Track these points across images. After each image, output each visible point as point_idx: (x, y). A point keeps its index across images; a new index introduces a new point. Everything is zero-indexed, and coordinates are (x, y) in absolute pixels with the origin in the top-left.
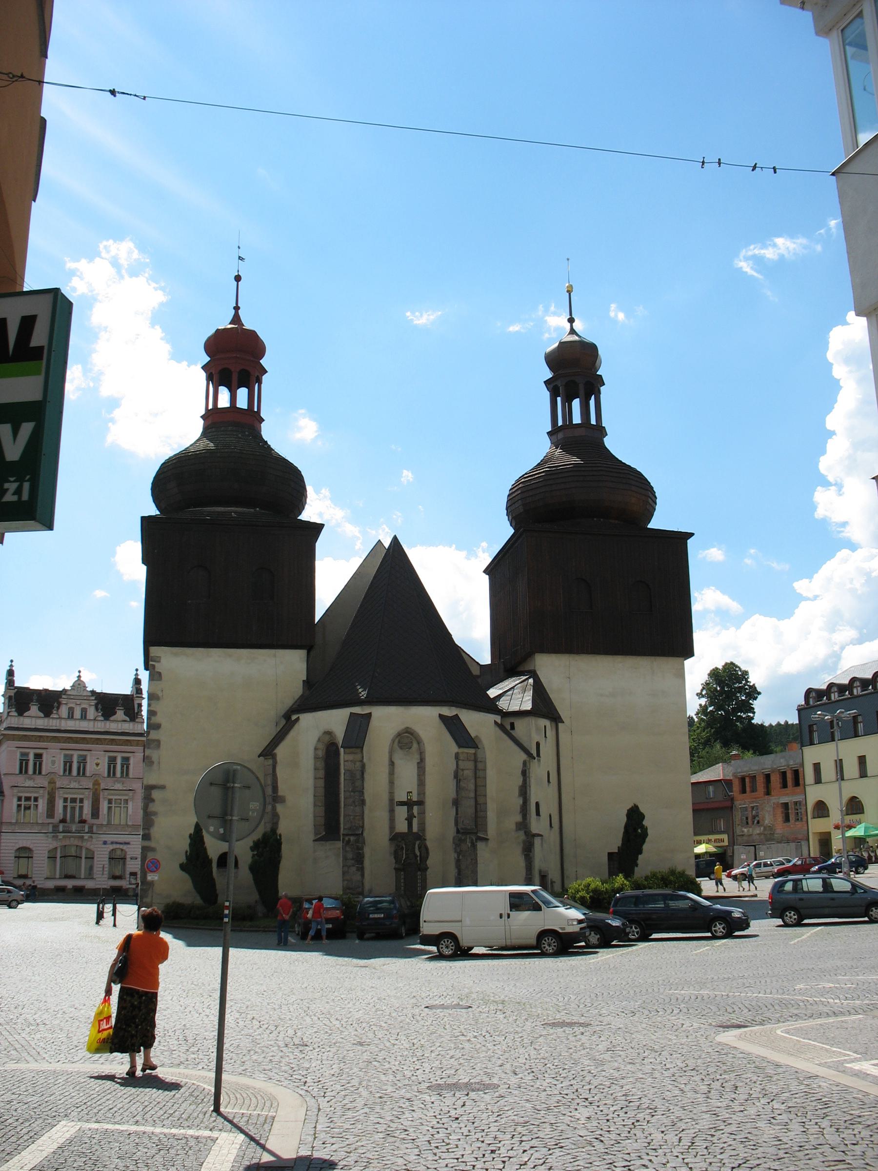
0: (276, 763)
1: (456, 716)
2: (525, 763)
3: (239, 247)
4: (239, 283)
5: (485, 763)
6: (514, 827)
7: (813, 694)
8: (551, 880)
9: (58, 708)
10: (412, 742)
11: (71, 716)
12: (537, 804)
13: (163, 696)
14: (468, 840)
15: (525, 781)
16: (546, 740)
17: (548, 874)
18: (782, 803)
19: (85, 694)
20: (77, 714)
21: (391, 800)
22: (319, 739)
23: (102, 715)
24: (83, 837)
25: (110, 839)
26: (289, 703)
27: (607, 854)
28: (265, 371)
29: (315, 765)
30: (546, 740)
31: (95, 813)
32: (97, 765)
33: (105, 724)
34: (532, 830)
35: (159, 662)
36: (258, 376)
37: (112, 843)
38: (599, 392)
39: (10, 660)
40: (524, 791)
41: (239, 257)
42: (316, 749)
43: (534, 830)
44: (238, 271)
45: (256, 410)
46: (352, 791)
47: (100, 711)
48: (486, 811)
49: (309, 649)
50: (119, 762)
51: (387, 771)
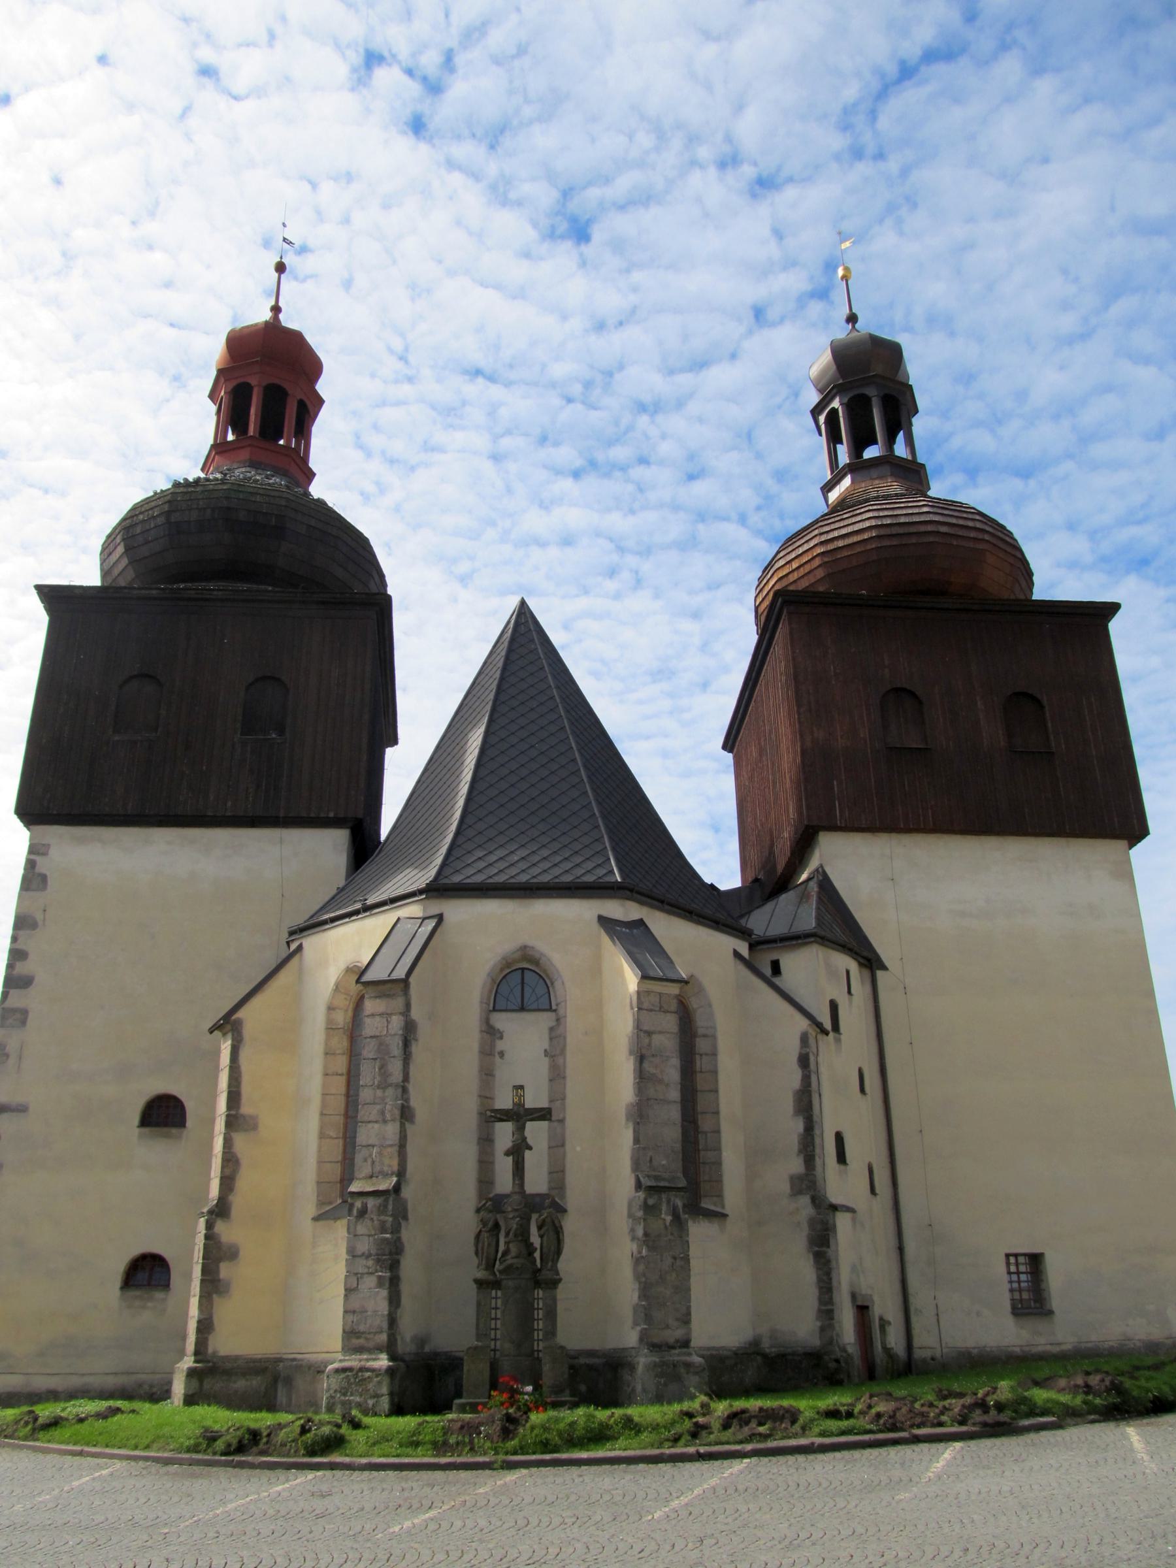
1: (640, 923)
2: (804, 1039)
4: (282, 275)
5: (714, 1037)
6: (786, 1187)
8: (881, 1319)
12: (839, 1138)
13: (44, 920)
14: (664, 1208)
15: (806, 1080)
16: (850, 1002)
17: (873, 1301)
22: (337, 987)
29: (326, 1044)
30: (850, 1002)
34: (828, 1195)
35: (45, 854)
38: (911, 424)
42: (331, 1008)
43: (834, 1197)
46: (378, 1087)
48: (718, 1149)
51: (476, 1046)
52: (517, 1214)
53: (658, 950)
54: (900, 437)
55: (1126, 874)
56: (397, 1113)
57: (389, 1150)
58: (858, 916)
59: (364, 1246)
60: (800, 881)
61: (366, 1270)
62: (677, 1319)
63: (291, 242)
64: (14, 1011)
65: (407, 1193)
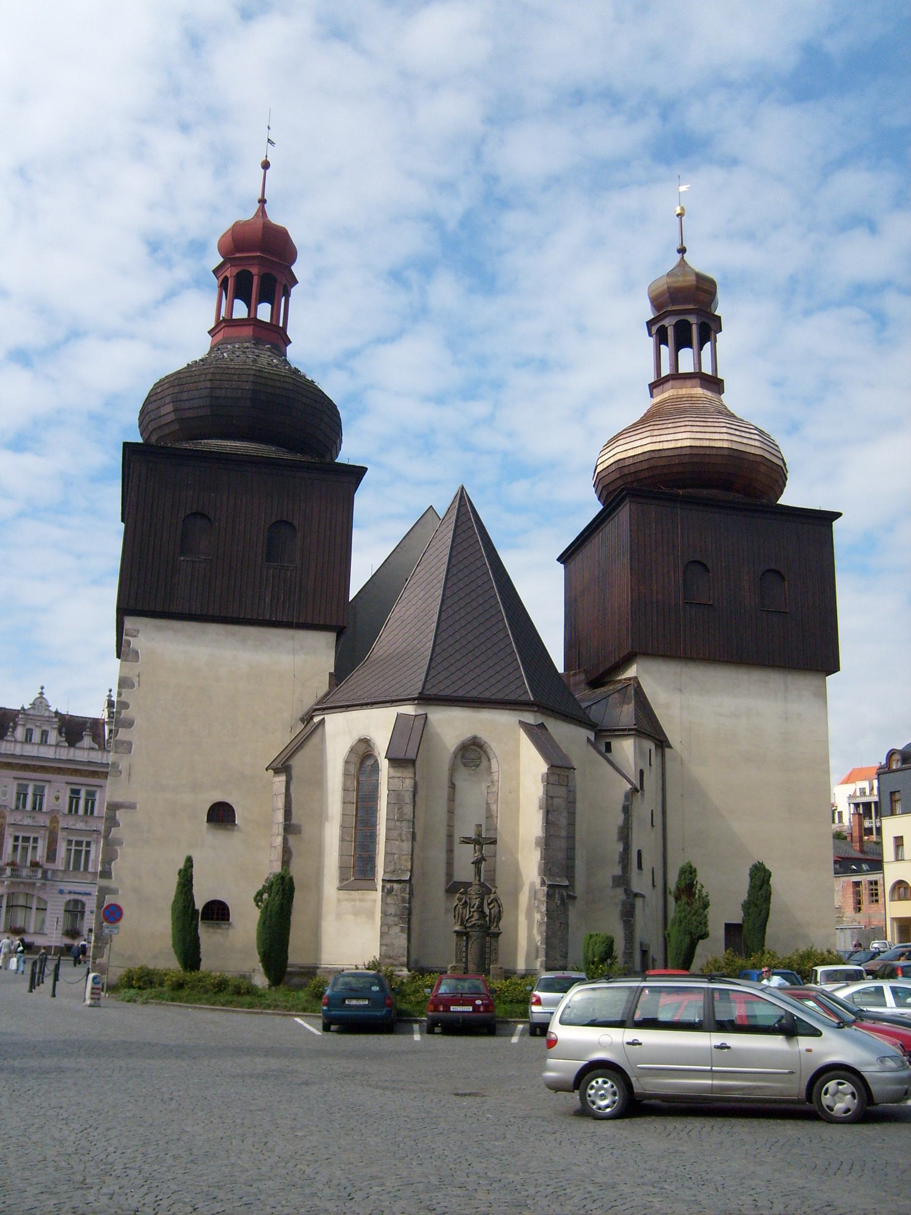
0: (291, 778)
3: (269, 128)
4: (267, 171)
6: (609, 882)
7: (897, 757)
9: (14, 728)
10: (480, 758)
11: (28, 739)
12: (639, 853)
18: (854, 882)
19: (47, 714)
20: (36, 737)
21: (450, 836)
22: (351, 750)
23: (67, 741)
24: (34, 884)
25: (67, 888)
26: (310, 702)
27: (724, 926)
28: (295, 282)
30: (650, 770)
31: (51, 856)
32: (57, 798)
33: (68, 753)
36: (285, 284)
37: (70, 892)
39: (40, 686)
40: (625, 834)
41: (269, 140)
42: (347, 762)
43: (636, 889)
44: (266, 157)
45: (281, 325)
47: (63, 735)
49: (340, 632)
50: (83, 795)
51: (446, 797)
52: (478, 896)
53: (550, 739)
54: (708, 346)
55: (822, 695)
56: (410, 836)
57: (405, 857)
58: (657, 712)
59: (392, 910)
60: (620, 678)
61: (394, 923)
62: (561, 956)
63: (273, 143)
64: (123, 742)
65: (413, 881)
